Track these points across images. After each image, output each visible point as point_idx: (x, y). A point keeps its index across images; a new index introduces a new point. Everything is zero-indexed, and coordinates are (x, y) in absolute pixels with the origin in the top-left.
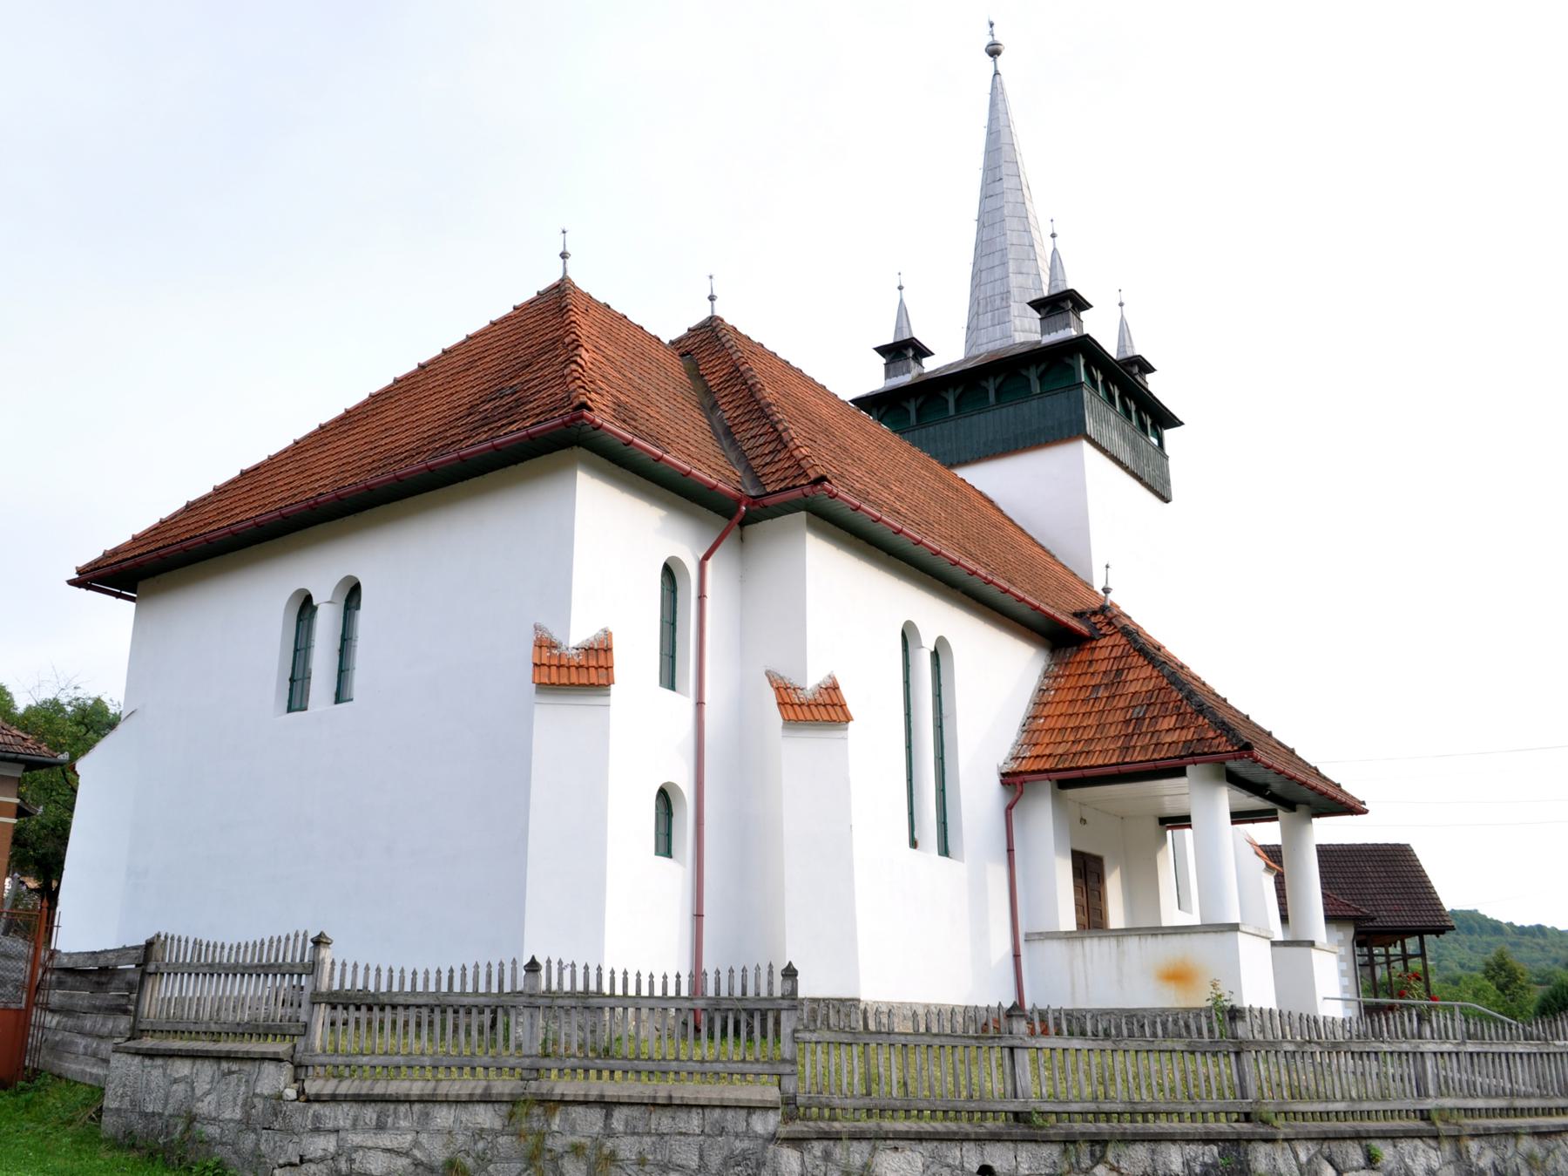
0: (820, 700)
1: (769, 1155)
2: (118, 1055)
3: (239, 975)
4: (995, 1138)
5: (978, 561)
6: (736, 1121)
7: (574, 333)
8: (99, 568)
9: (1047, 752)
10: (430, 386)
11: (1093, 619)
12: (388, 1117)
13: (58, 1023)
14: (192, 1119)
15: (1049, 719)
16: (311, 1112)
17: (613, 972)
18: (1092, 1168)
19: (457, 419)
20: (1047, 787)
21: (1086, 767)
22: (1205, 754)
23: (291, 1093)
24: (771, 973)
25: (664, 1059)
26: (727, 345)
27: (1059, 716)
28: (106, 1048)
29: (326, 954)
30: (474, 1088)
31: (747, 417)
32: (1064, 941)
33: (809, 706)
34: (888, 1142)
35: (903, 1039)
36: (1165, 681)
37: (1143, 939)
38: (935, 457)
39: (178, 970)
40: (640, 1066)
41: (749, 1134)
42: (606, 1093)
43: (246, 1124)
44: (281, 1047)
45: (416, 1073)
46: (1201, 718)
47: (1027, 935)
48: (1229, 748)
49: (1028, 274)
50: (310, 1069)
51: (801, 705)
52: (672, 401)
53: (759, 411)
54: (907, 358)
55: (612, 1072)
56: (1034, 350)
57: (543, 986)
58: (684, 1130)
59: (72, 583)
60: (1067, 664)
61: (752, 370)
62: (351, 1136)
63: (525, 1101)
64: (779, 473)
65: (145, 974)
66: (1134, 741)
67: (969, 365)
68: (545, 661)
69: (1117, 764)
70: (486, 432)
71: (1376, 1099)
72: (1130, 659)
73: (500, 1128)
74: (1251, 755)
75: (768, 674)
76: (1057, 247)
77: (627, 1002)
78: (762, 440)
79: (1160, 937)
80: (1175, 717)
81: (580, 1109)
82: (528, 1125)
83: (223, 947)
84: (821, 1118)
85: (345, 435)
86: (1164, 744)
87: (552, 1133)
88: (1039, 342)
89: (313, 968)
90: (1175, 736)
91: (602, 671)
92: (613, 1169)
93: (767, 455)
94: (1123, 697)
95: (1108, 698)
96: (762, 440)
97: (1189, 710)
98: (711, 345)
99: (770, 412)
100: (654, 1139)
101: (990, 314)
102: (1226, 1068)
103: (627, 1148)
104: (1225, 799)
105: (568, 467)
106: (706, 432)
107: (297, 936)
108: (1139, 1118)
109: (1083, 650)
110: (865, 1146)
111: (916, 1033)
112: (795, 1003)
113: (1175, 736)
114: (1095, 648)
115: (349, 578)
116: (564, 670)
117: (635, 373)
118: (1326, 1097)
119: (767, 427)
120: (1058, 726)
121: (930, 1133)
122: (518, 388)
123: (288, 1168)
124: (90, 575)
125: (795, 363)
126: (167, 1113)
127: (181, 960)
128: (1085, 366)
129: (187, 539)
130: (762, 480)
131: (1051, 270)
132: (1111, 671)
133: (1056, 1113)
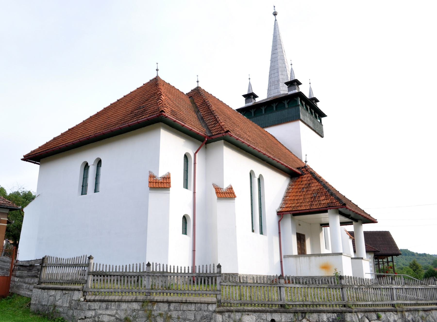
0: (227, 192)
1: (213, 316)
3: (68, 267)
4: (275, 312)
5: (270, 153)
6: (204, 307)
7: (160, 91)
8: (30, 156)
9: (290, 206)
11: (302, 170)
13: (18, 280)
14: (55, 306)
16: (88, 304)
17: (170, 266)
18: (302, 320)
19: (128, 115)
20: (290, 215)
21: (300, 210)
22: (333, 206)
23: (82, 299)
24: (214, 266)
25: (185, 290)
26: (202, 95)
27: (293, 196)
28: (31, 287)
29: (92, 261)
30: (133, 298)
31: (207, 114)
33: (224, 193)
34: (246, 313)
35: (250, 285)
36: (322, 186)
38: (259, 125)
39: (51, 265)
41: (208, 310)
42: (169, 299)
43: (70, 308)
44: (80, 287)
45: (117, 294)
46: (332, 197)
47: (284, 256)
48: (340, 205)
50: (88, 293)
51: (222, 193)
52: (187, 110)
53: (211, 113)
55: (170, 294)
58: (190, 309)
59: (22, 160)
60: (295, 182)
61: (209, 101)
63: (146, 302)
67: (268, 100)
68: (152, 181)
70: (136, 118)
71: (380, 301)
72: (312, 180)
73: (140, 309)
75: (213, 184)
77: (175, 274)
78: (211, 121)
79: (321, 256)
81: (162, 304)
83: (64, 259)
84: (227, 306)
87: (154, 310)
88: (287, 94)
89: (88, 265)
90: (324, 202)
93: (213, 124)
94: (310, 191)
95: (306, 191)
96: (211, 121)
97: (329, 194)
99: (214, 113)
101: (274, 86)
102: (338, 293)
103: (174, 314)
104: (338, 219)
105: (158, 128)
107: (84, 256)
108: (315, 306)
109: (300, 178)
111: (254, 283)
113: (324, 202)
114: (303, 177)
115: (98, 158)
116: (157, 184)
119: (213, 117)
120: (293, 199)
121: (257, 310)
123: (81, 320)
125: (220, 99)
126: (48, 305)
127: (52, 263)
128: (300, 100)
129: (54, 148)
130: (211, 131)
132: (307, 184)
133: (292, 305)
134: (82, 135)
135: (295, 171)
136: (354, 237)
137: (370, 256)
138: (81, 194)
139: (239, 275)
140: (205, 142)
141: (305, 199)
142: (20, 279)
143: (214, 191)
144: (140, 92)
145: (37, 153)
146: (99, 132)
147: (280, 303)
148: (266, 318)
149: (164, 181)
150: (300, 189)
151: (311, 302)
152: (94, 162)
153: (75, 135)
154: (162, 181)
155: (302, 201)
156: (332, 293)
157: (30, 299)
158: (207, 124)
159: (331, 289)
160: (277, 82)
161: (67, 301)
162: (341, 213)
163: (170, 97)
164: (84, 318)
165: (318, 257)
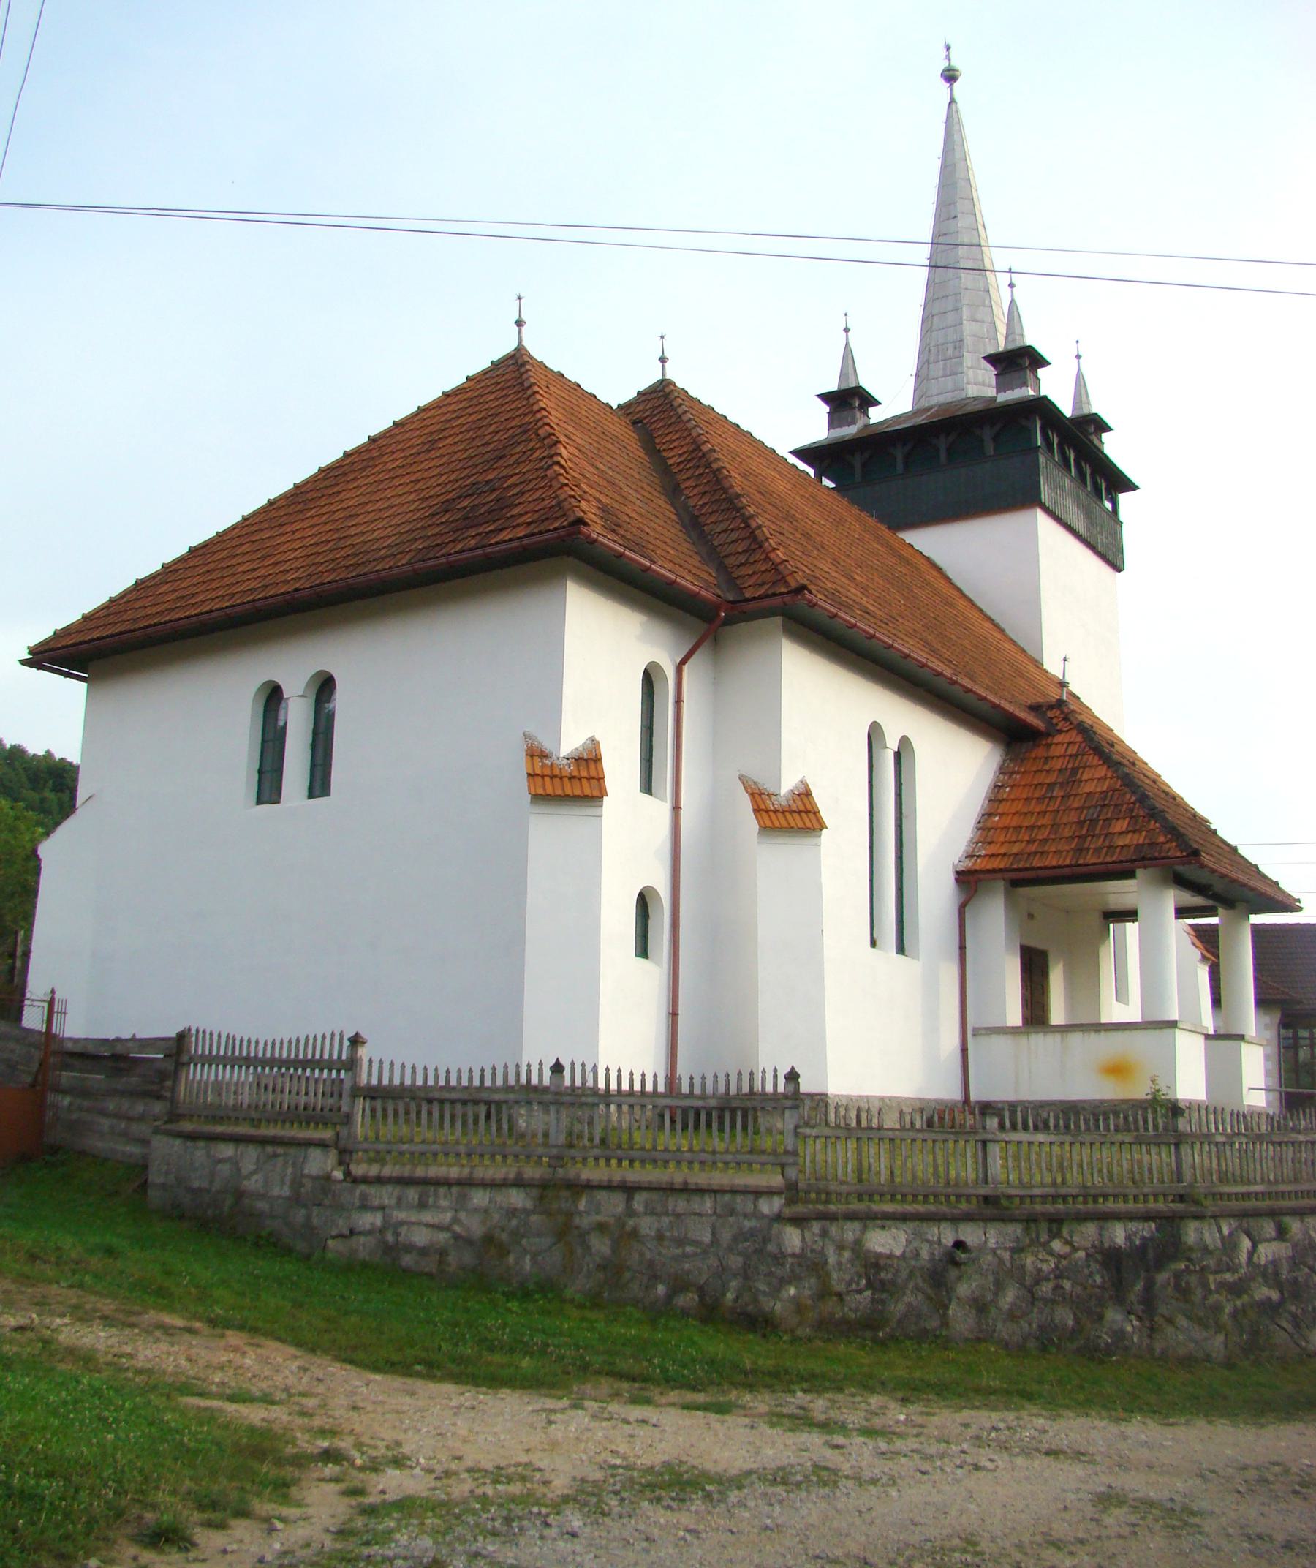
0: (794, 808)
1: (774, 1231)
4: (968, 1218)
5: (940, 658)
7: (548, 424)
9: (1002, 851)
11: (1050, 714)
13: (71, 1104)
14: (240, 1195)
15: (1004, 817)
16: (358, 1192)
17: (607, 1069)
20: (1000, 886)
21: (1040, 868)
23: (338, 1174)
24: (775, 1076)
26: (685, 418)
27: (1014, 814)
29: (363, 1052)
32: (1010, 1037)
33: (783, 812)
36: (1119, 782)
38: (881, 519)
39: (210, 1060)
41: (756, 1214)
42: (627, 1179)
43: (296, 1199)
44: (326, 1134)
45: (451, 1159)
46: (1152, 822)
48: (1178, 854)
51: (776, 811)
53: (729, 503)
54: (851, 407)
56: (989, 410)
57: (567, 1082)
59: (24, 662)
60: (1022, 760)
64: (756, 577)
66: (1087, 843)
67: (919, 420)
68: (538, 771)
70: (473, 537)
71: (1290, 1182)
72: (1085, 757)
75: (741, 778)
76: (1015, 298)
78: (734, 536)
79: (1102, 1033)
84: (818, 1201)
87: (580, 1213)
88: (994, 399)
89: (351, 1064)
90: (1126, 840)
91: (594, 782)
94: (1078, 798)
95: (1063, 797)
96: (734, 536)
97: (1141, 813)
99: (740, 505)
100: (671, 1218)
103: (647, 1226)
104: (1171, 898)
105: (555, 577)
107: (333, 1035)
108: (1090, 1200)
109: (1039, 746)
111: (903, 1129)
112: (798, 1102)
113: (1126, 840)
114: (1051, 745)
115: (321, 673)
116: (557, 781)
117: (603, 461)
120: (1014, 824)
121: (912, 1214)
126: (214, 1189)
127: (237, 1053)
128: (1041, 428)
130: (738, 582)
131: (1008, 325)
132: (1066, 769)
135: (1024, 721)
136: (1218, 957)
137: (1267, 1019)
138: (255, 801)
141: (1059, 825)
143: (746, 804)
145: (85, 642)
147: (982, 1191)
148: (939, 1239)
149: (579, 770)
150: (1039, 787)
152: (307, 686)
154: (575, 773)
155: (1045, 836)
156: (1146, 1158)
157: (145, 1167)
160: (955, 348)
162: (1180, 881)
164: (348, 1232)
165: (1093, 1034)
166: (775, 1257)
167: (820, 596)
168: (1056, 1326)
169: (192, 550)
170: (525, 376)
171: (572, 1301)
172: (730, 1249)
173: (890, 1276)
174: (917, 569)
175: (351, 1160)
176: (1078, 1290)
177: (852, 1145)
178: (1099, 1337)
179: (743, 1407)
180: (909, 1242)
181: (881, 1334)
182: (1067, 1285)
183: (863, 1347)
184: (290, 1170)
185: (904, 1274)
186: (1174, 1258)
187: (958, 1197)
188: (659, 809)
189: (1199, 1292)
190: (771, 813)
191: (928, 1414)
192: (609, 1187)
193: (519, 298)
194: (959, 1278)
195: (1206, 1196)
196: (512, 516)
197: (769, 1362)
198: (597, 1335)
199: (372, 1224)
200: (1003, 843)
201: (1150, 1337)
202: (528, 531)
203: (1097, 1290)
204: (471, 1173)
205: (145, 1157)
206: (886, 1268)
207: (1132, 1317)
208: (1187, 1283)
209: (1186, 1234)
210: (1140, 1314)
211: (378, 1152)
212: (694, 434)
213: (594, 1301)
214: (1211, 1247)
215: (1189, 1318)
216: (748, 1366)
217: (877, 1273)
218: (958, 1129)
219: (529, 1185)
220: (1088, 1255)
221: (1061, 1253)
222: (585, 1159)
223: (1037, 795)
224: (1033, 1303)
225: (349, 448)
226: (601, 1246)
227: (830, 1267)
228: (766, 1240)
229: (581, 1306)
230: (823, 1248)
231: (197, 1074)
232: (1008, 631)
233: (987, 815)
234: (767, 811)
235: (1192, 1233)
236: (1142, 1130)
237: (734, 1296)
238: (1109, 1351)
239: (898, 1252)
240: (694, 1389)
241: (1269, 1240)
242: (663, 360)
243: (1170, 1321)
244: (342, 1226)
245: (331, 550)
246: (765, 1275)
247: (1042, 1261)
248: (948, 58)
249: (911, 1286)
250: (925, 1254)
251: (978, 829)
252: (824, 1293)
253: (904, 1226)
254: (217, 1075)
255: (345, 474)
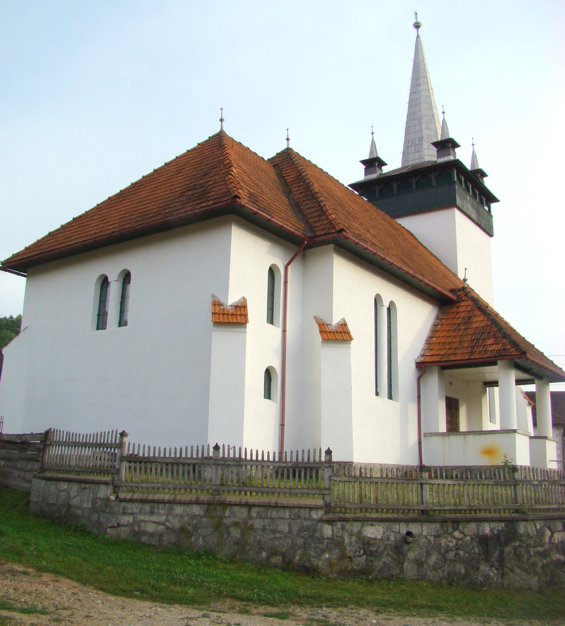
0: (339, 330)
1: (319, 527)
2: (35, 479)
3: (87, 448)
4: (414, 520)
5: (408, 266)
6: (304, 513)
7: (229, 159)
8: (10, 262)
9: (437, 353)
10: (161, 181)
11: (459, 293)
12: (155, 509)
13: (4, 465)
14: (69, 507)
15: (438, 338)
16: (122, 506)
18: (453, 532)
19: (175, 199)
20: (436, 369)
21: (454, 360)
22: (506, 356)
23: (113, 498)
25: (274, 487)
28: (29, 476)
29: (126, 440)
30: (192, 498)
31: (306, 198)
33: (333, 333)
34: (369, 522)
35: (376, 480)
36: (490, 323)
37: (475, 436)
38: (387, 213)
40: (261, 490)
41: (310, 519)
43: (94, 509)
44: (108, 478)
46: (505, 340)
47: (425, 434)
49: (431, 129)
50: (121, 488)
51: (330, 332)
52: (272, 190)
54: (375, 166)
55: (251, 493)
56: (434, 166)
57: (221, 455)
58: (282, 517)
60: (447, 313)
61: (307, 175)
62: (139, 516)
63: (214, 504)
65: (46, 446)
67: (404, 171)
68: (217, 312)
69: (468, 359)
70: (190, 206)
72: (474, 312)
73: (203, 514)
74: (526, 357)
75: (315, 317)
76: (445, 118)
77: (258, 463)
78: (313, 210)
79: (482, 435)
80: (493, 339)
81: (237, 508)
82: (215, 514)
83: (80, 435)
84: (340, 512)
85: (121, 203)
86: (488, 351)
87: (226, 517)
88: (436, 161)
89: (120, 446)
90: (493, 348)
91: (243, 317)
92: (252, 532)
93: (315, 217)
94: (471, 329)
95: (464, 329)
96: (313, 210)
97: (500, 336)
98: (288, 162)
99: (317, 197)
100: (269, 520)
101: (413, 148)
102: (510, 491)
103: (258, 524)
104: (513, 375)
105: (226, 224)
106: (288, 205)
107: (113, 432)
108: (473, 512)
110: (359, 524)
111: (382, 477)
113: (493, 348)
116: (226, 316)
117: (255, 177)
118: (549, 503)
119: (315, 204)
120: (442, 341)
121: (387, 519)
122: (204, 185)
123: (113, 528)
124: (7, 265)
125: (325, 170)
126: (58, 504)
127: (61, 440)
129: (52, 250)
130: (314, 229)
132: (466, 317)
133: (439, 510)
134: (99, 230)
137: (557, 432)
139: (354, 465)
140: (303, 247)
141: (462, 342)
142: (7, 463)
144: (193, 158)
146: (127, 226)
147: (421, 507)
148: (399, 531)
151: (467, 506)
153: (86, 230)
154: (234, 313)
155: (456, 346)
156: (500, 492)
157: (29, 494)
158: (306, 216)
159: (499, 486)
160: (419, 141)
161: (88, 499)
162: (518, 367)
163: (244, 168)
164: (116, 525)
165: (478, 435)
166: (318, 539)
167: (350, 234)
168: (456, 573)
169: (74, 219)
170: (222, 141)
171: (221, 560)
172: (297, 535)
173: (375, 549)
174: (401, 233)
175: (119, 490)
176: (467, 555)
177: (357, 484)
178: (477, 578)
179: (295, 615)
180: (384, 532)
181: (370, 577)
182: (462, 553)
183: (361, 583)
184: (92, 495)
185: (382, 548)
186: (513, 540)
187: (409, 510)
188: (276, 331)
189: (526, 556)
190: (328, 333)
191: (388, 619)
192: (240, 505)
193: (222, 109)
194: (409, 550)
195: (529, 510)
196: (208, 197)
197: (313, 591)
198: (229, 577)
199: (128, 521)
200: (437, 350)
201: (502, 578)
202: (214, 202)
203: (476, 555)
204: (175, 498)
205: (30, 488)
206: (373, 544)
207: (494, 569)
208: (520, 552)
209: (519, 528)
210: (497, 567)
211: (132, 487)
212: (299, 169)
213: (232, 560)
214: (531, 535)
215: (521, 569)
216: (301, 594)
217: (369, 547)
218: (409, 478)
219: (202, 504)
220: (472, 539)
221: (459, 538)
222: (229, 491)
223: (453, 329)
224: (445, 562)
225: (145, 174)
226: (235, 533)
227: (346, 544)
228: (315, 531)
229: (225, 562)
230: (342, 535)
231: (54, 451)
232: (442, 261)
233: (430, 337)
234: (326, 332)
235: (522, 528)
236: (498, 478)
237: (299, 558)
238: (482, 585)
239: (379, 537)
240: (272, 605)
241: (559, 532)
242: (288, 139)
243: (512, 571)
244: (114, 522)
245: (130, 216)
246: (314, 548)
247: (449, 541)
248: (416, 18)
249: (385, 553)
250: (392, 538)
251: (426, 344)
252: (343, 556)
253: (382, 525)
254: (78, 452)
255: (142, 185)
